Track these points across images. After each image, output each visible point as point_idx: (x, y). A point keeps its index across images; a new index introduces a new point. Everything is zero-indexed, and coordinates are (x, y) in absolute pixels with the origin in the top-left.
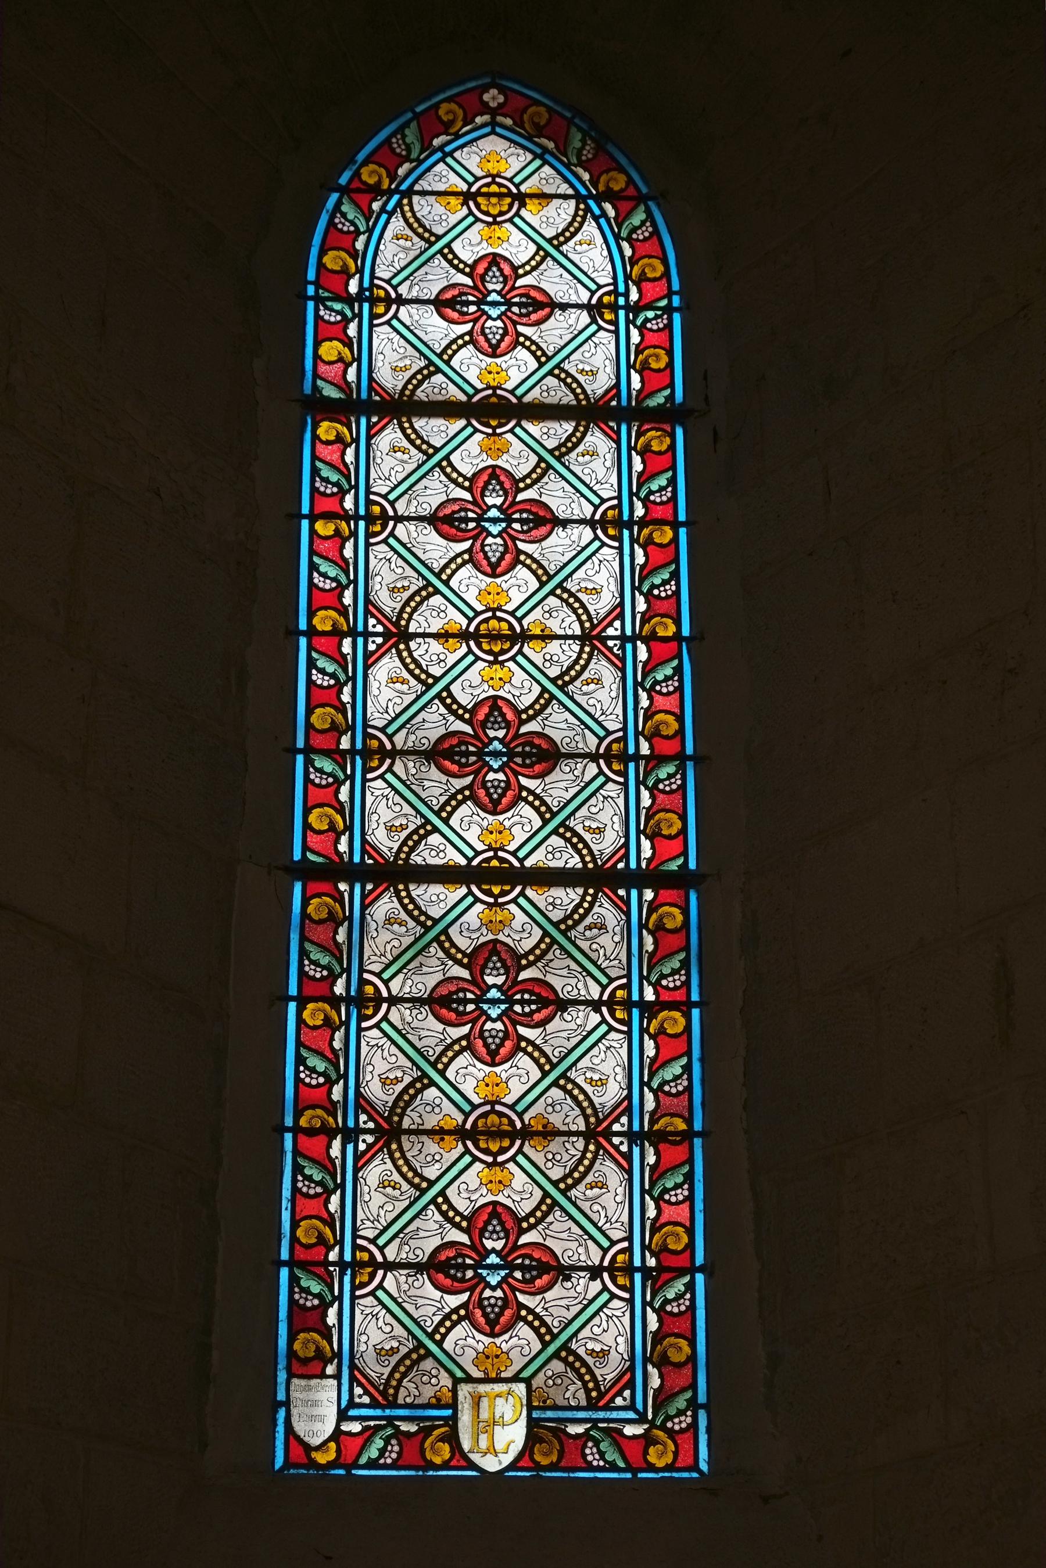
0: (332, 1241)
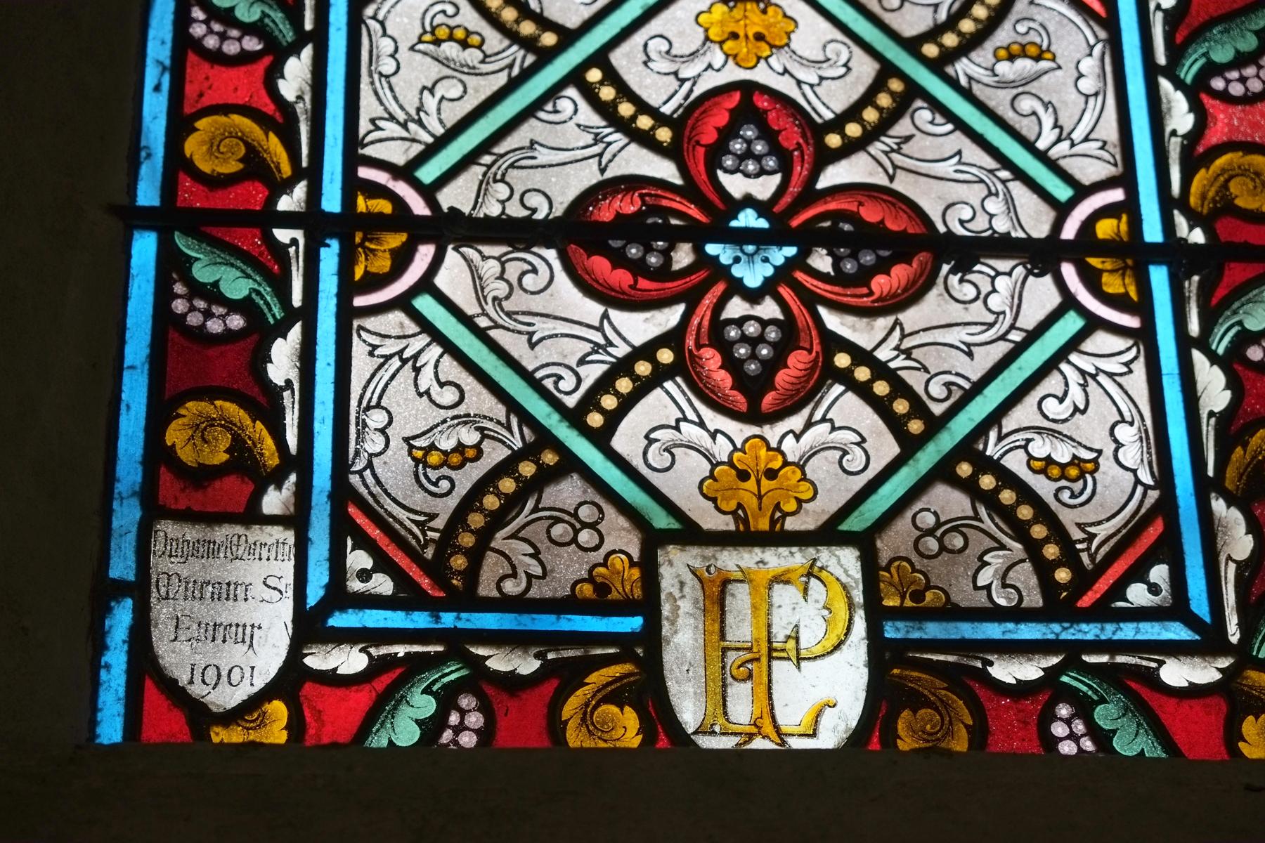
0: (286, 170)
